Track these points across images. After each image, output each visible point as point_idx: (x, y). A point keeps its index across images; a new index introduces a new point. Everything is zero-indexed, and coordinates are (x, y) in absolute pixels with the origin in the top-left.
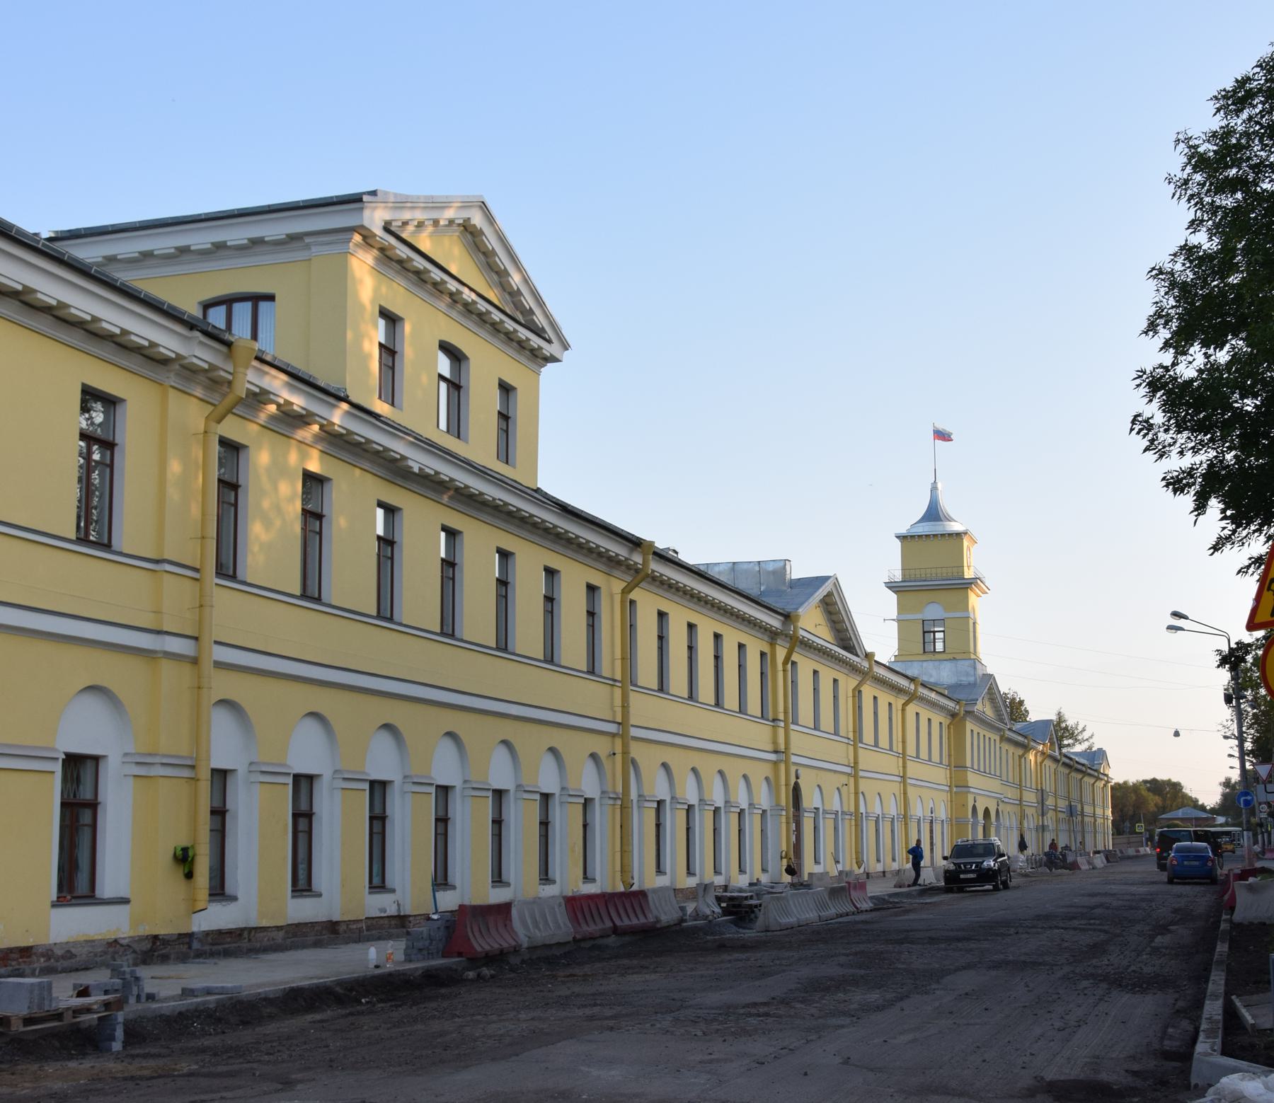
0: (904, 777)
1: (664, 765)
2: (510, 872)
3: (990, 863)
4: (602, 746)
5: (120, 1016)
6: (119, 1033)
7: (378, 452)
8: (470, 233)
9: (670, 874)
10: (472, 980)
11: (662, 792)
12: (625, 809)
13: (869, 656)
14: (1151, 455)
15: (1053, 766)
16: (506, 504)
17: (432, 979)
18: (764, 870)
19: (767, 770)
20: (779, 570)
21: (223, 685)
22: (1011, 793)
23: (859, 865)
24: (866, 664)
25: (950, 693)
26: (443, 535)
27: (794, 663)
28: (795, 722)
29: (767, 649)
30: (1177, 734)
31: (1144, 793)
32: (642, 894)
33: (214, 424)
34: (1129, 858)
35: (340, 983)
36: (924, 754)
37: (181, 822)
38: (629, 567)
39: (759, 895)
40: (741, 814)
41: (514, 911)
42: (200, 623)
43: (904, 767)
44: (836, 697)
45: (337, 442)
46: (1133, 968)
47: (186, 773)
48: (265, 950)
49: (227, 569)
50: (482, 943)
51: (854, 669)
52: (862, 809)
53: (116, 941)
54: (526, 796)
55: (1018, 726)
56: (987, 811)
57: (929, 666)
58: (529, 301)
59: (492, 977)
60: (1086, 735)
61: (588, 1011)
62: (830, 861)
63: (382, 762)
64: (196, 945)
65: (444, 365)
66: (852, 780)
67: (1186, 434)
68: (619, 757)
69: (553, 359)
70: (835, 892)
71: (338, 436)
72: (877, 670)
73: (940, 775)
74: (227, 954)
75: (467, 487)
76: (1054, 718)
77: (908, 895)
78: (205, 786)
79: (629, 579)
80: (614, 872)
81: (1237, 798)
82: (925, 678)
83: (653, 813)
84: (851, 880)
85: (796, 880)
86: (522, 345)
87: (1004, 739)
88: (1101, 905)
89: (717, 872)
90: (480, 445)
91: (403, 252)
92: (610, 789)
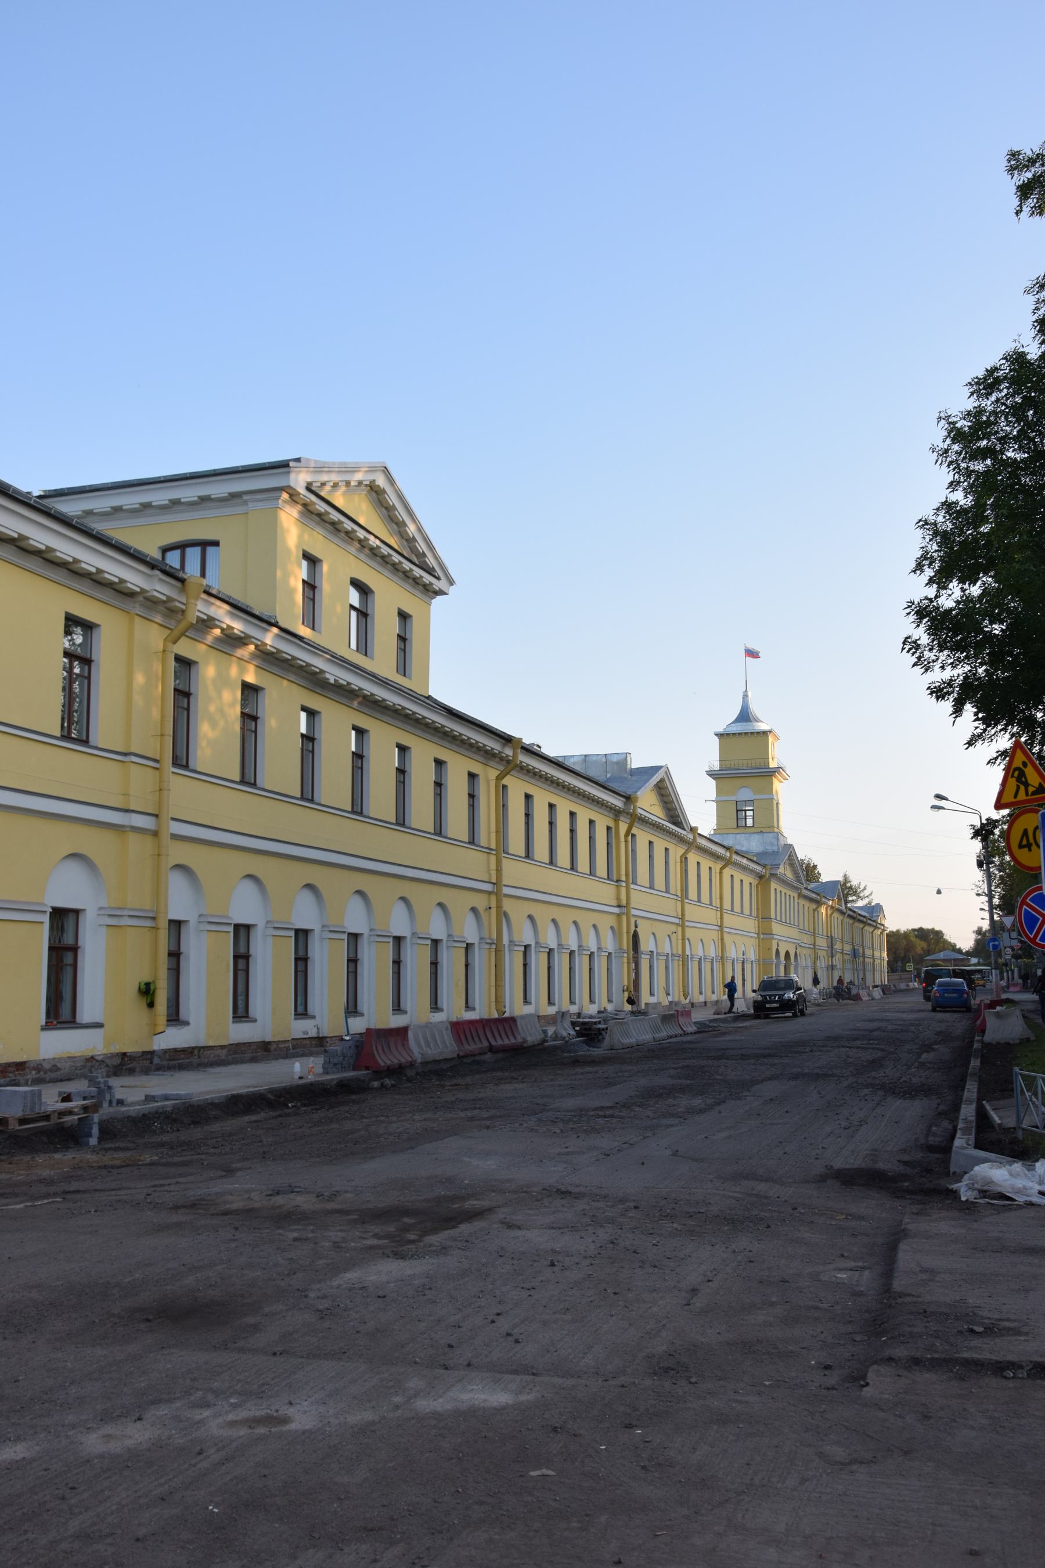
0: (721, 926)
1: (530, 917)
2: (407, 1002)
3: (790, 995)
4: (480, 902)
5: (96, 1118)
6: (95, 1131)
7: (301, 667)
8: (375, 491)
9: (534, 1004)
10: (377, 1089)
11: (528, 938)
12: (499, 951)
13: (693, 830)
14: (918, 670)
15: (840, 917)
16: (404, 708)
17: (345, 1088)
18: (610, 1001)
19: (612, 921)
21: (178, 853)
22: (807, 939)
24: (691, 836)
25: (758, 859)
26: (353, 733)
27: (633, 836)
28: (634, 883)
29: (611, 824)
30: (939, 892)
31: (913, 939)
32: (512, 1020)
33: (170, 645)
34: (901, 991)
35: (271, 1091)
36: (737, 908)
37: (144, 962)
38: (502, 759)
39: (605, 1021)
41: (410, 1034)
42: (160, 803)
43: (722, 918)
44: (667, 863)
45: (269, 659)
46: (904, 1079)
47: (149, 923)
48: (212, 1064)
49: (181, 760)
50: (384, 1060)
51: (681, 840)
52: (688, 952)
53: (92, 1057)
54: (420, 941)
55: (812, 886)
56: (787, 954)
57: (741, 838)
58: (422, 547)
59: (393, 1086)
60: (866, 893)
61: (469, 1114)
62: (662, 994)
64: (156, 1060)
65: (354, 597)
66: (680, 929)
67: (946, 652)
68: (494, 911)
69: (441, 593)
70: (666, 1019)
73: (750, 925)
74: (181, 1068)
75: (373, 695)
77: (724, 1021)
78: (163, 934)
79: (502, 768)
80: (490, 1002)
81: (986, 943)
82: (738, 848)
83: (521, 955)
84: (678, 1008)
85: (635, 1009)
86: (416, 582)
87: (801, 896)
88: (879, 1029)
89: (572, 1002)
90: (383, 660)
91: (321, 507)
92: (487, 936)
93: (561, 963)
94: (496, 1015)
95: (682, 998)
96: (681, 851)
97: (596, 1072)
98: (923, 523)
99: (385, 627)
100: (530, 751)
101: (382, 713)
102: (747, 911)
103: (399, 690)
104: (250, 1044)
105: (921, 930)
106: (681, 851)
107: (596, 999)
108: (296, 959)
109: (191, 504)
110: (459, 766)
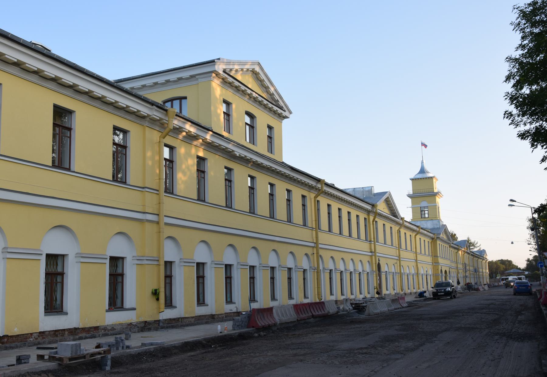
0: (416, 260)
1: (332, 257)
2: (278, 295)
3: (449, 289)
4: (309, 251)
5: (109, 356)
6: (109, 363)
7: (224, 149)
8: (254, 73)
9: (332, 296)
10: (257, 337)
11: (331, 267)
12: (318, 272)
13: (402, 219)
14: (512, 126)
15: (468, 255)
16: (271, 167)
17: (242, 337)
18: (369, 293)
19: (368, 258)
20: (370, 190)
21: (168, 231)
22: (454, 265)
23: (402, 291)
24: (401, 222)
25: (431, 231)
26: (249, 178)
27: (376, 222)
28: (377, 242)
29: (366, 217)
30: (512, 243)
31: (499, 264)
32: (323, 303)
33: (162, 139)
34: (496, 286)
35: (205, 339)
36: (423, 252)
37: (155, 281)
38: (316, 189)
39: (366, 302)
40: (360, 273)
41: (274, 311)
42: (159, 209)
43: (416, 257)
44: (391, 233)
45: (210, 146)
46: (514, 330)
47: (156, 263)
48: (187, 325)
49: (170, 190)
50: (261, 322)
51: (397, 223)
52: (402, 271)
53: (131, 323)
54: (282, 269)
55: (455, 242)
56: (446, 271)
57: (423, 222)
58: (277, 97)
59: (265, 335)
60: (478, 245)
61: (295, 352)
62: (392, 289)
63: (229, 258)
64: (161, 324)
65: (248, 120)
66: (398, 261)
67: (526, 117)
68: (315, 255)
69: (286, 117)
70: (393, 301)
71: (209, 143)
72: (405, 223)
73: (429, 259)
74: (173, 327)
75: (257, 161)
76: (466, 239)
77: (420, 301)
78: (162, 268)
79: (316, 193)
80: (315, 295)
81: (531, 265)
82: (422, 226)
83: (328, 274)
84: (399, 296)
85: (380, 296)
86: (275, 112)
87: (450, 246)
88: (492, 304)
89: (352, 294)
90: (261, 147)
91: (230, 79)
92: (312, 266)
93: (346, 277)
94: (318, 301)
95: (401, 291)
96: (397, 228)
97: (361, 327)
98: (510, 59)
99: (262, 133)
100: (332, 186)
101: (262, 169)
102: (427, 253)
103: (269, 159)
104: (205, 316)
105: (502, 260)
106: (397, 228)
107: (362, 292)
108: (226, 278)
109: (175, 81)
110: (297, 193)
